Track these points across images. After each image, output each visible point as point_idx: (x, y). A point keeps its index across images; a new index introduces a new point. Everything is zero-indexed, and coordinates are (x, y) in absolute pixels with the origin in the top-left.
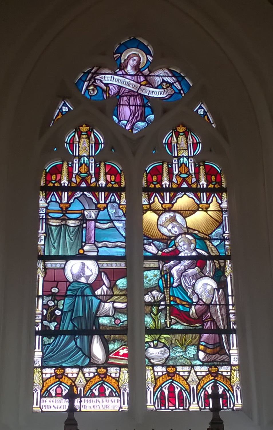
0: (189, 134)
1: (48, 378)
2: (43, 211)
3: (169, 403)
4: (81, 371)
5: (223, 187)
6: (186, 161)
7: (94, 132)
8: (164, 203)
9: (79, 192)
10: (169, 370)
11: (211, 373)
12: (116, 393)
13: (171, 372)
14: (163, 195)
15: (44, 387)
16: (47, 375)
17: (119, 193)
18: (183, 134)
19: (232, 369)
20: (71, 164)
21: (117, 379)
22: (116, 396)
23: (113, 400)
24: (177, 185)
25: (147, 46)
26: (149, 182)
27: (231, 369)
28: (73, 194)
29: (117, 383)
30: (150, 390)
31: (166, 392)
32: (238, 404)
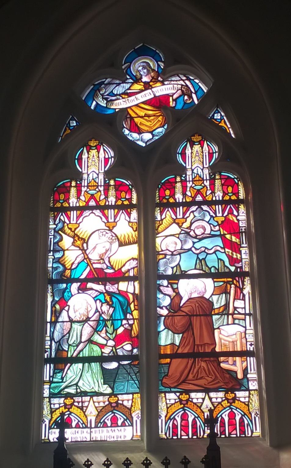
0: (205, 142)
1: (172, 404)
2: (51, 233)
3: (182, 432)
4: (207, 394)
5: (133, 204)
6: (201, 173)
7: (103, 146)
8: (108, 222)
9: (193, 207)
10: (227, 396)
11: (227, 399)
12: (84, 425)
13: (183, 399)
14: (214, 208)
15: (168, 414)
16: (55, 405)
17: (129, 210)
18: (95, 148)
19: (251, 394)
20: (184, 177)
21: (247, 403)
22: (129, 425)
23: (119, 430)
24: (85, 203)
25: (155, 51)
26: (162, 197)
27: (250, 394)
28: (188, 209)
29: (247, 407)
30: (45, 423)
31: (226, 419)
32: (256, 431)
